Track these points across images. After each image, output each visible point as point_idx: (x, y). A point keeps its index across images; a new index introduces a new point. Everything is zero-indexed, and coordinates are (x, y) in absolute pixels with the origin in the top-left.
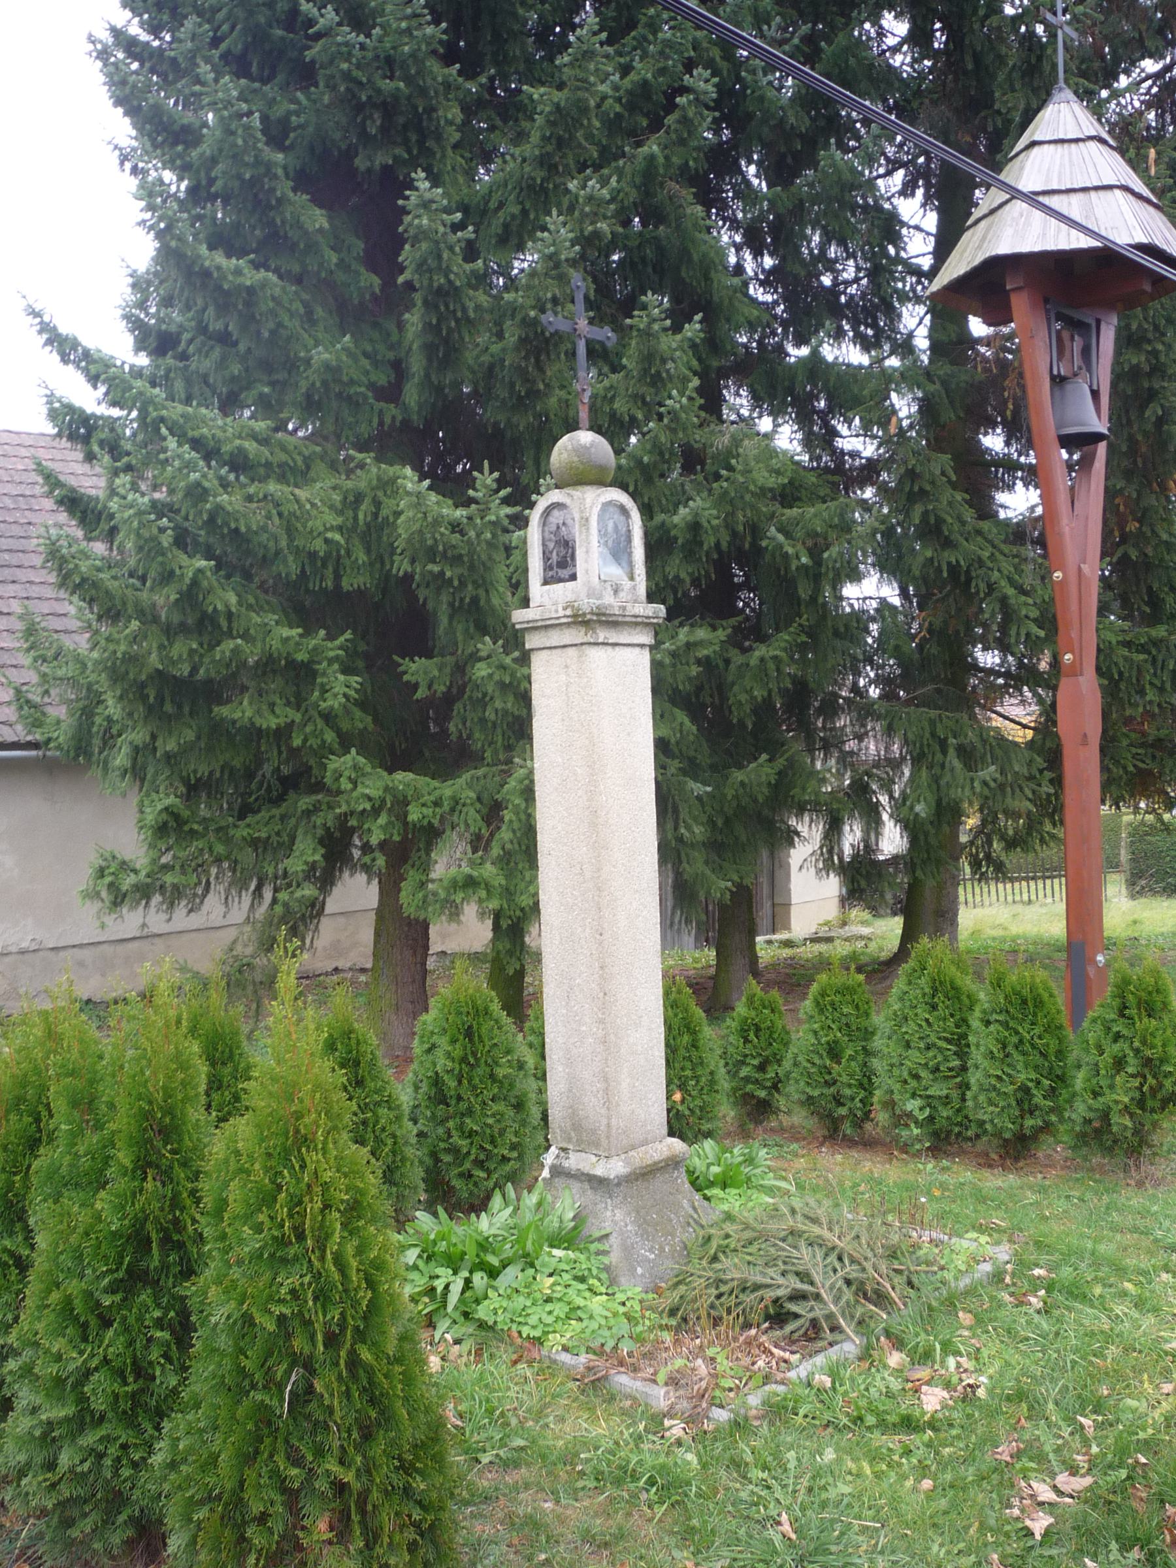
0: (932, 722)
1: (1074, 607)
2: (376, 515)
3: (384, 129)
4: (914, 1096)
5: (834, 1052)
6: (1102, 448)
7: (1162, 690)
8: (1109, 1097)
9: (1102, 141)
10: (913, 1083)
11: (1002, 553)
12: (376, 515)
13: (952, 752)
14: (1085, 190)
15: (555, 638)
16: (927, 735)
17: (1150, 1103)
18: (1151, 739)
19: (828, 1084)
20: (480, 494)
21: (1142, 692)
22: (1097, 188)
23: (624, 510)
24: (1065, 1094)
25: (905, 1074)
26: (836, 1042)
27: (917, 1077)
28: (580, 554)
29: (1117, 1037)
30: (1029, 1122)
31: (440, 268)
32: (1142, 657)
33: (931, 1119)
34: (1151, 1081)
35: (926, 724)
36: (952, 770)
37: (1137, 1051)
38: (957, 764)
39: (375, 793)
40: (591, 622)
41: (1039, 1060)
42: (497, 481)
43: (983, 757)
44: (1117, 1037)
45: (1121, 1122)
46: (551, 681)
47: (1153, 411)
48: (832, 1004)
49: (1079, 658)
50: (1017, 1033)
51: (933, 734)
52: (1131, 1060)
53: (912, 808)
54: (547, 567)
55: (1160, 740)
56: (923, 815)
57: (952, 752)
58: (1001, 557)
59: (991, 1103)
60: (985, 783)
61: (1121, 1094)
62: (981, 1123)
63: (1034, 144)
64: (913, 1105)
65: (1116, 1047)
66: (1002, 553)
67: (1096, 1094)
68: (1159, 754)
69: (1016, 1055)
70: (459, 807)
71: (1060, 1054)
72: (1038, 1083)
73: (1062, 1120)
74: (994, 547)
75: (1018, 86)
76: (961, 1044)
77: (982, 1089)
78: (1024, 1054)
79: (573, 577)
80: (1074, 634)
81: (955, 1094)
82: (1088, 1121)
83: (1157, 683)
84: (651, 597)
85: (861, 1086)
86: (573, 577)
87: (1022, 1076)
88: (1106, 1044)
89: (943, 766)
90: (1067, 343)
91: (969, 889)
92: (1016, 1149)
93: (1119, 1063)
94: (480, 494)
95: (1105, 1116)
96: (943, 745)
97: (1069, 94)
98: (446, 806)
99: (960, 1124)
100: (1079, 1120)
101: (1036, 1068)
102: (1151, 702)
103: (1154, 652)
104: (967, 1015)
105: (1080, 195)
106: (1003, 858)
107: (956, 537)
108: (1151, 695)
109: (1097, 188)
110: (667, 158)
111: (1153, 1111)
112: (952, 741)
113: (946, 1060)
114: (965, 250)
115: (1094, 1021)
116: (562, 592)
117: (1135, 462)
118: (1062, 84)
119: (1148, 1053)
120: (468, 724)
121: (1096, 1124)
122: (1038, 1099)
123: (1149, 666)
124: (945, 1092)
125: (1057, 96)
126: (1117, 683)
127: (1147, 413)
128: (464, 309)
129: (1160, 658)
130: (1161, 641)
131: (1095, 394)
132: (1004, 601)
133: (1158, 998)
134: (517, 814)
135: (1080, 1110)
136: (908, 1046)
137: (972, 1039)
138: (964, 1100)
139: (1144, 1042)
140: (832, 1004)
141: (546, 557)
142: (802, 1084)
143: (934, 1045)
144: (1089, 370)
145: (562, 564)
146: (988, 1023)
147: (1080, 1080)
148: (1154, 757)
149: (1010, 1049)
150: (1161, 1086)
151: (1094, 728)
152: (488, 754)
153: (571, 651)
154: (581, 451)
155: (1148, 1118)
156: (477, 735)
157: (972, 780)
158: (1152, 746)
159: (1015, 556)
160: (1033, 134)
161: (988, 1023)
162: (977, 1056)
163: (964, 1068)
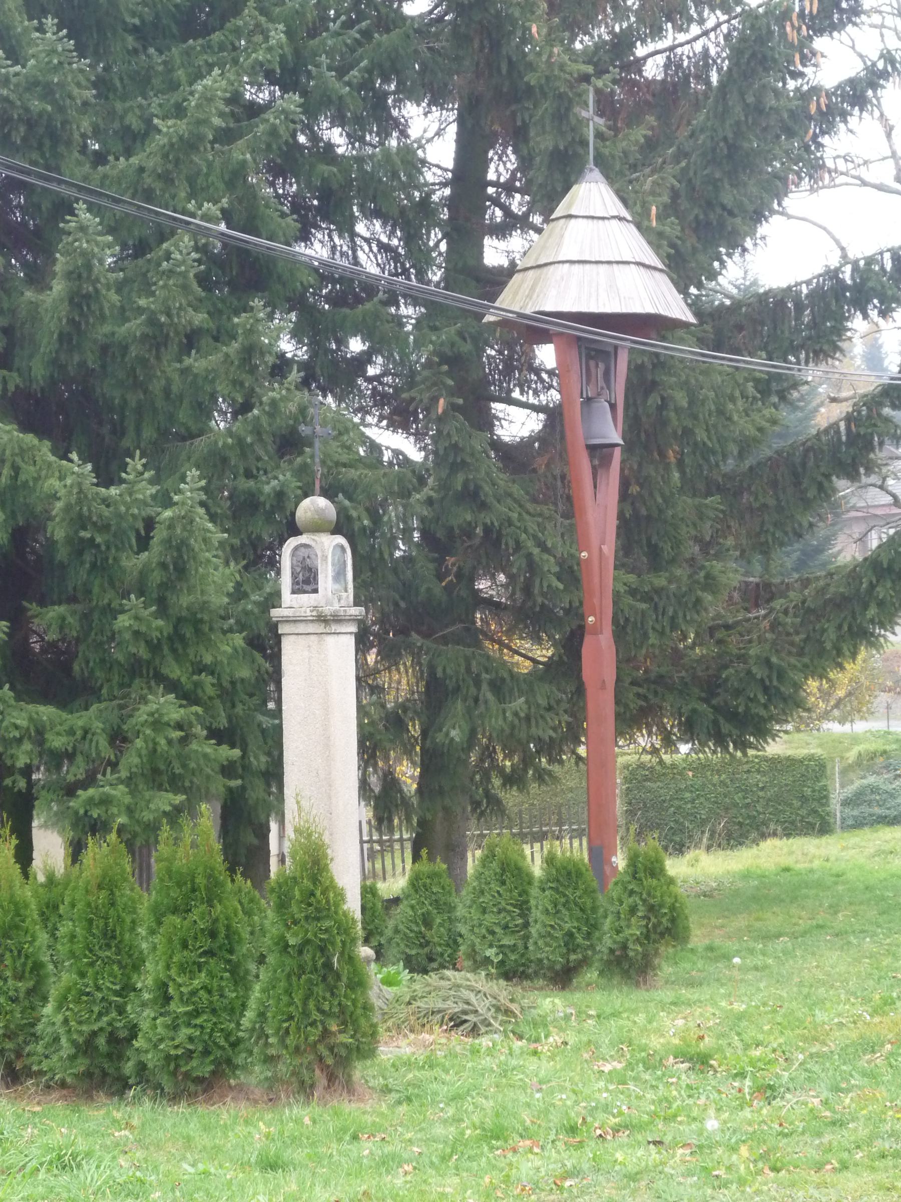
0: (468, 661)
1: (596, 580)
2: (15, 477)
3: (24, 139)
4: (491, 946)
5: (427, 922)
6: (617, 452)
7: (662, 633)
8: (627, 932)
9: (621, 219)
10: (490, 937)
11: (528, 513)
12: (15, 477)
13: (485, 687)
14: (609, 263)
15: (301, 628)
16: (462, 669)
17: (653, 936)
18: (653, 675)
19: (422, 946)
20: (131, 477)
21: (645, 636)
22: (618, 263)
23: (342, 548)
24: (597, 934)
25: (484, 931)
26: (429, 913)
27: (493, 933)
28: (321, 577)
29: (632, 893)
30: (573, 957)
31: (89, 277)
32: (644, 606)
33: (502, 963)
34: (653, 920)
35: (462, 661)
36: (486, 702)
37: (644, 901)
38: (490, 696)
39: (23, 722)
40: (326, 620)
41: (578, 913)
42: (144, 465)
43: (511, 691)
44: (632, 893)
45: (635, 949)
46: (294, 654)
47: (654, 400)
48: (425, 886)
49: (600, 620)
50: (565, 895)
51: (468, 670)
52: (641, 908)
53: (447, 734)
54: (295, 582)
55: (661, 677)
56: (457, 739)
57: (485, 687)
58: (527, 517)
59: (547, 944)
60: (516, 714)
61: (635, 930)
62: (540, 961)
63: (570, 217)
64: (490, 952)
65: (631, 900)
66: (528, 513)
67: (618, 932)
68: (659, 689)
69: (564, 911)
70: (89, 736)
71: (594, 909)
72: (579, 929)
73: (595, 952)
74: (521, 506)
75: (548, 128)
76: (523, 907)
77: (541, 936)
78: (569, 909)
79: (315, 591)
80: (596, 601)
81: (520, 943)
82: (612, 951)
83: (658, 627)
84: (356, 604)
85: (448, 945)
86: (315, 591)
87: (567, 926)
88: (625, 896)
89: (476, 700)
90: (593, 370)
91: (398, 854)
92: (563, 977)
93: (633, 910)
94: (131, 477)
95: (624, 947)
96: (478, 683)
97: (597, 174)
98: (79, 733)
99: (523, 965)
100: (606, 951)
101: (578, 919)
102: (653, 645)
103: (656, 599)
104: (527, 887)
105: (606, 266)
106: (501, 795)
107: (491, 500)
108: (653, 639)
109: (618, 263)
110: (254, 160)
111: (655, 941)
112: (485, 676)
113: (513, 919)
114: (516, 293)
115: (616, 884)
116: (306, 600)
117: (638, 435)
118: (592, 166)
119: (652, 901)
120: (91, 664)
121: (618, 953)
122: (579, 940)
123: (651, 612)
124: (512, 942)
125: (589, 176)
126: (624, 628)
127: (649, 402)
128: (101, 309)
129: (661, 605)
130: (662, 589)
131: (613, 407)
132: (529, 556)
133: (657, 865)
134: (146, 741)
135: (607, 941)
136: (484, 911)
137: (533, 902)
138: (526, 948)
139: (649, 894)
140: (425, 886)
141: (294, 575)
142: (402, 946)
143: (505, 910)
144: (609, 388)
145: (306, 580)
146: (544, 890)
147: (607, 924)
148: (656, 693)
149: (560, 907)
150: (660, 923)
151: (610, 674)
152: (104, 691)
153: (313, 637)
154: (319, 511)
155: (650, 947)
156: (98, 674)
157: (504, 712)
158: (654, 682)
159: (540, 515)
160: (570, 205)
161: (544, 890)
162: (536, 914)
163: (526, 925)
